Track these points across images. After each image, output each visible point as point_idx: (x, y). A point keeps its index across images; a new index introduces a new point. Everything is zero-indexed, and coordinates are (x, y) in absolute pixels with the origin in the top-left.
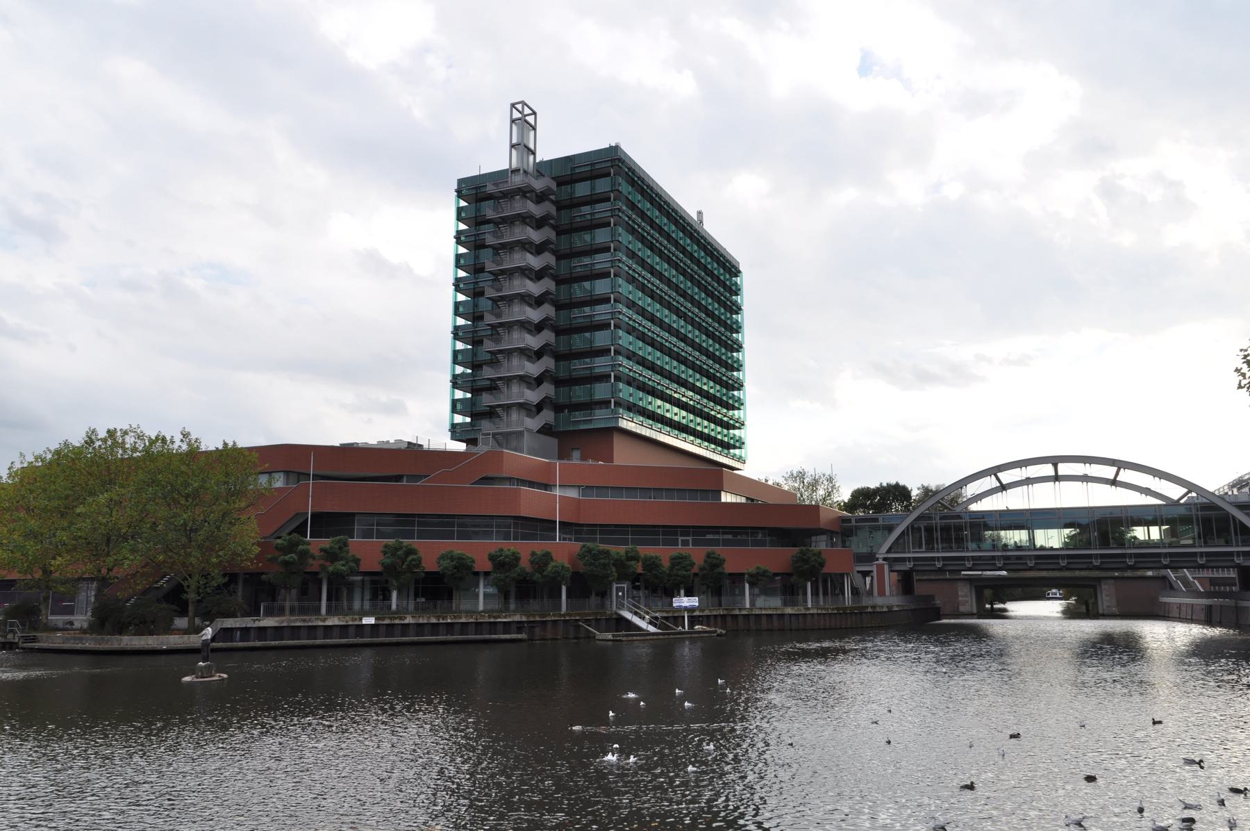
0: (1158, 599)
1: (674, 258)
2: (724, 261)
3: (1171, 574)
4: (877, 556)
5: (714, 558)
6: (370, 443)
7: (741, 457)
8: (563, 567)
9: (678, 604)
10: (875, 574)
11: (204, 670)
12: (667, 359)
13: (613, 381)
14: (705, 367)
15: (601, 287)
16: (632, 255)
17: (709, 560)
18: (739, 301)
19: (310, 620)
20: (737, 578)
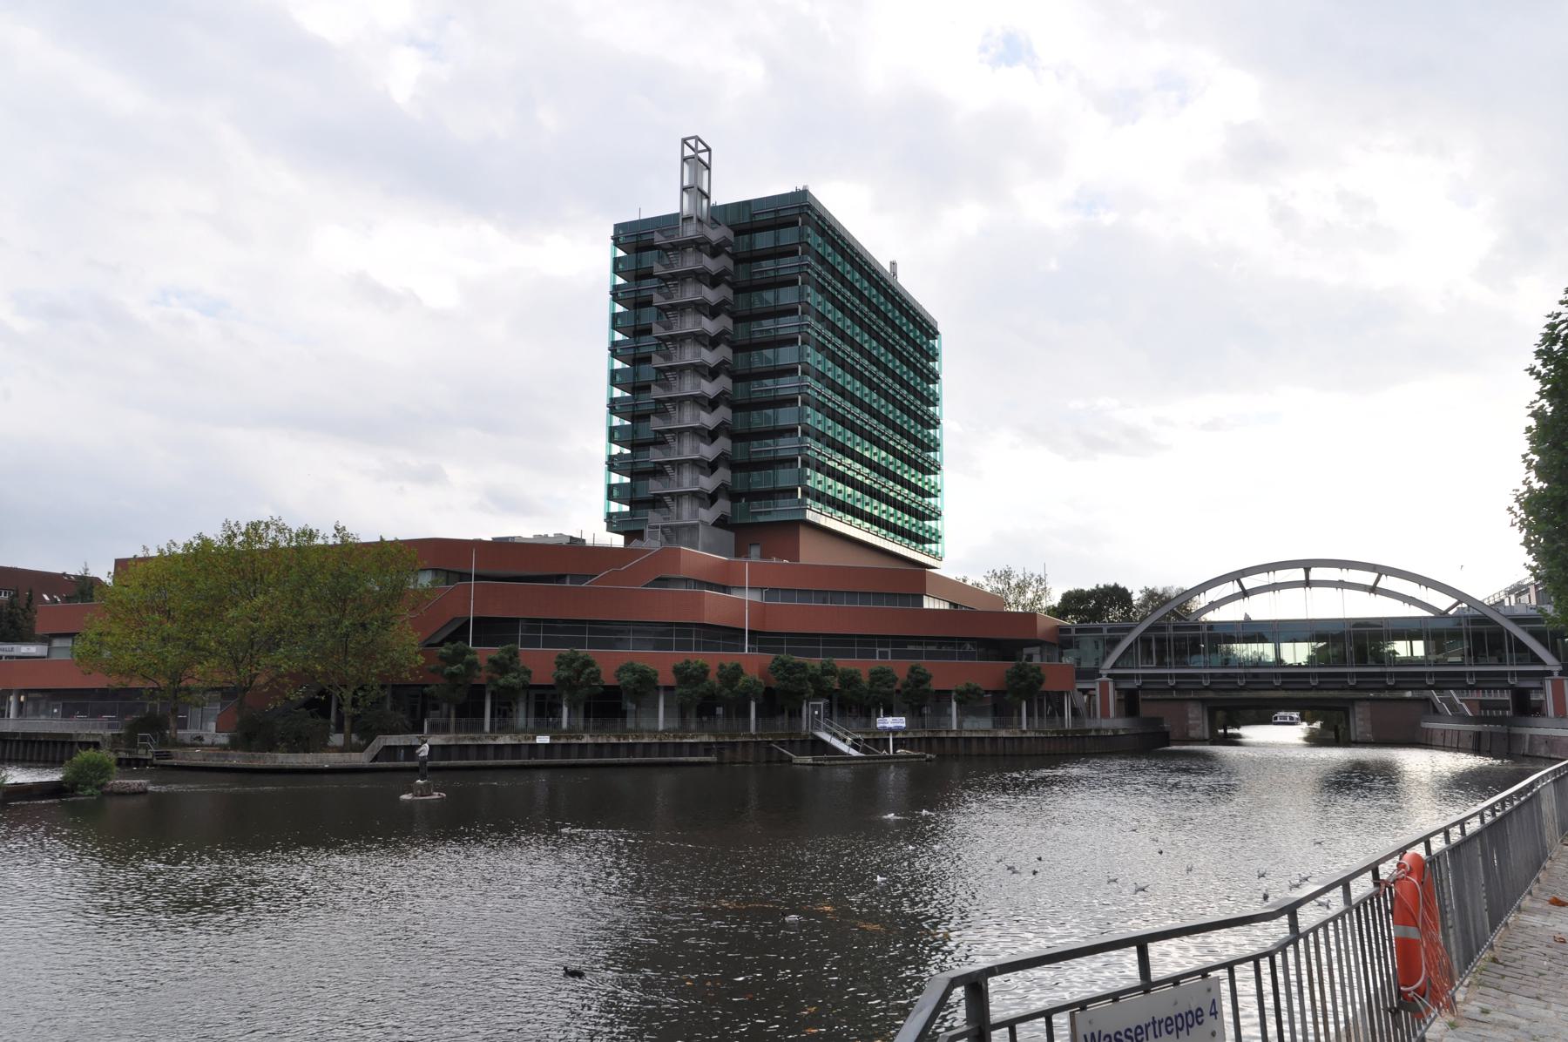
0: (1420, 724)
1: (840, 297)
2: (907, 308)
3: (1435, 696)
4: (1101, 672)
5: (918, 672)
6: (524, 536)
7: (937, 553)
8: (755, 681)
9: (882, 725)
10: (1097, 692)
11: (423, 788)
12: (840, 428)
13: (799, 466)
14: (858, 422)
15: (786, 356)
16: (821, 318)
17: (914, 676)
18: (937, 368)
19: (479, 739)
20: (943, 696)
